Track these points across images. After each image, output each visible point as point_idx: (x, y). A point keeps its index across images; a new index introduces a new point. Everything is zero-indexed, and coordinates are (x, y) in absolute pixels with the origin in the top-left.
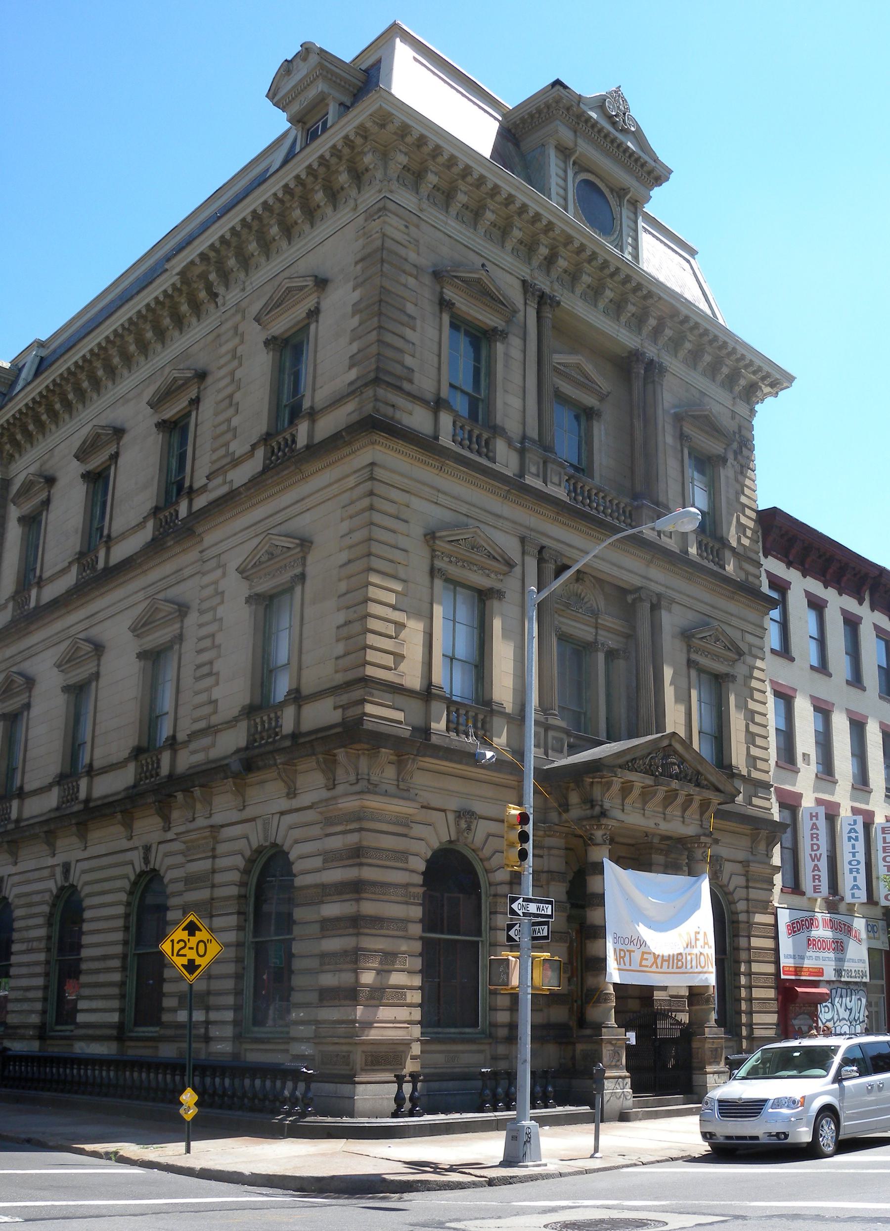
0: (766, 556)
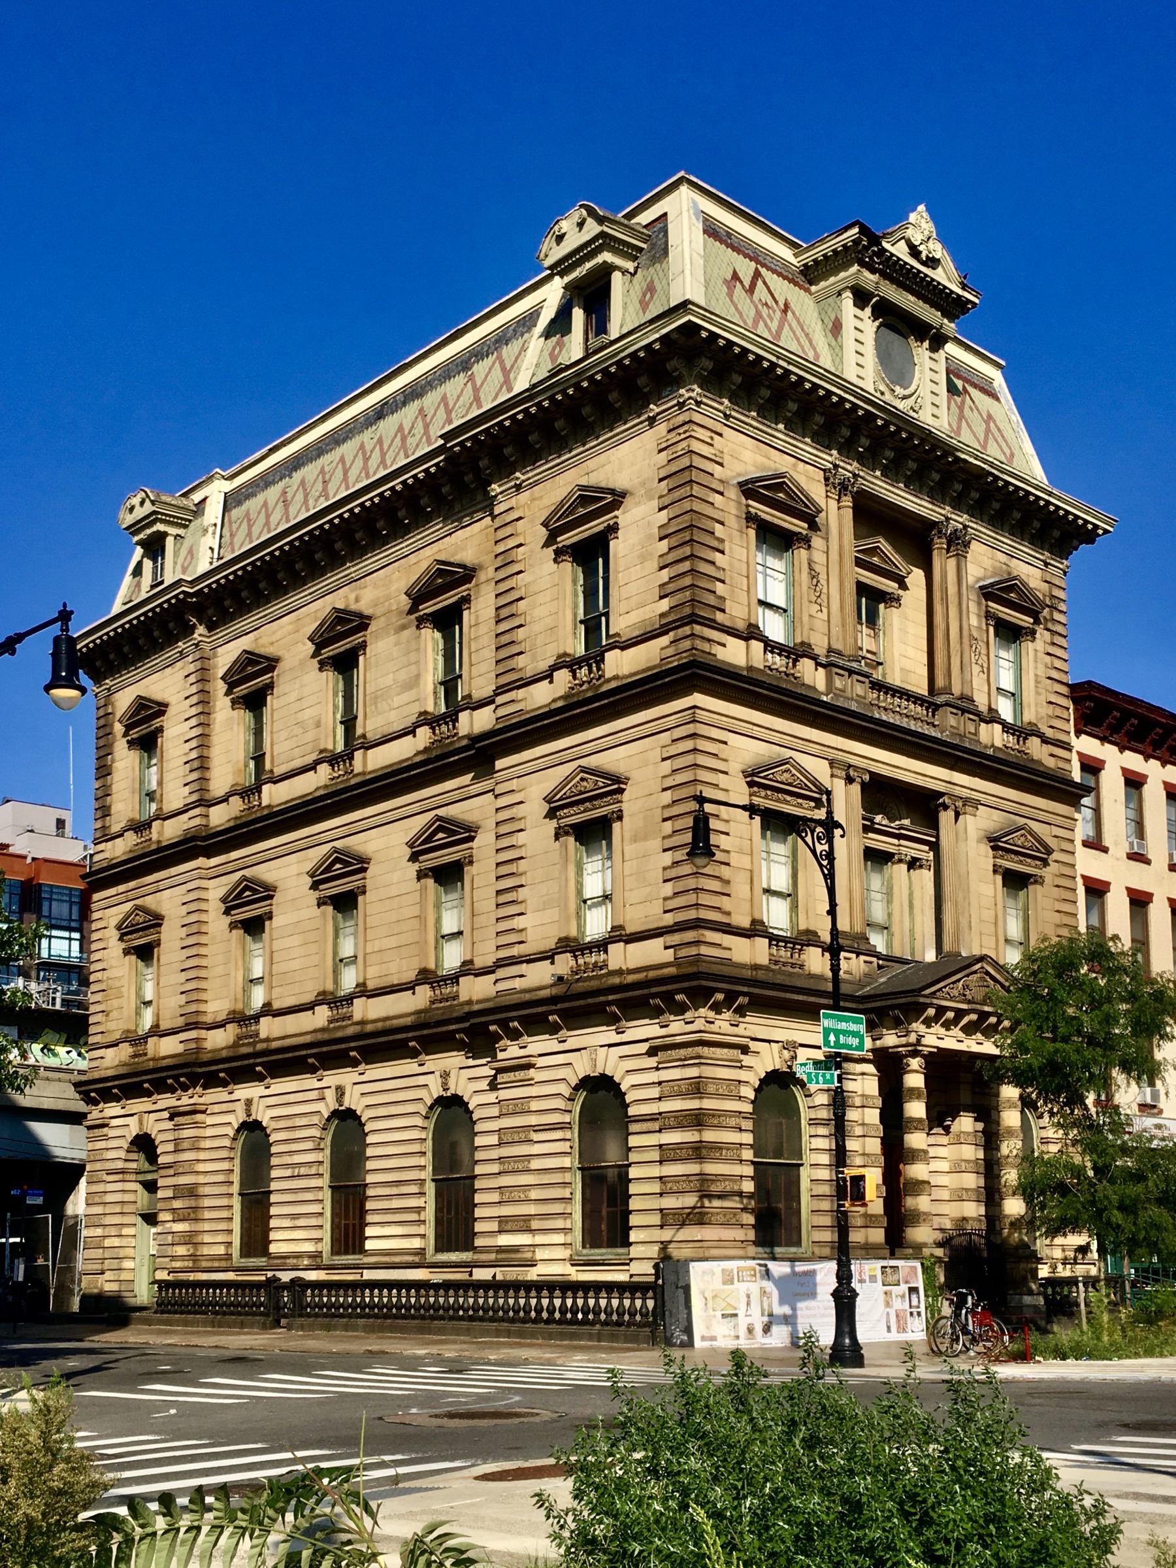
0: (1078, 733)
